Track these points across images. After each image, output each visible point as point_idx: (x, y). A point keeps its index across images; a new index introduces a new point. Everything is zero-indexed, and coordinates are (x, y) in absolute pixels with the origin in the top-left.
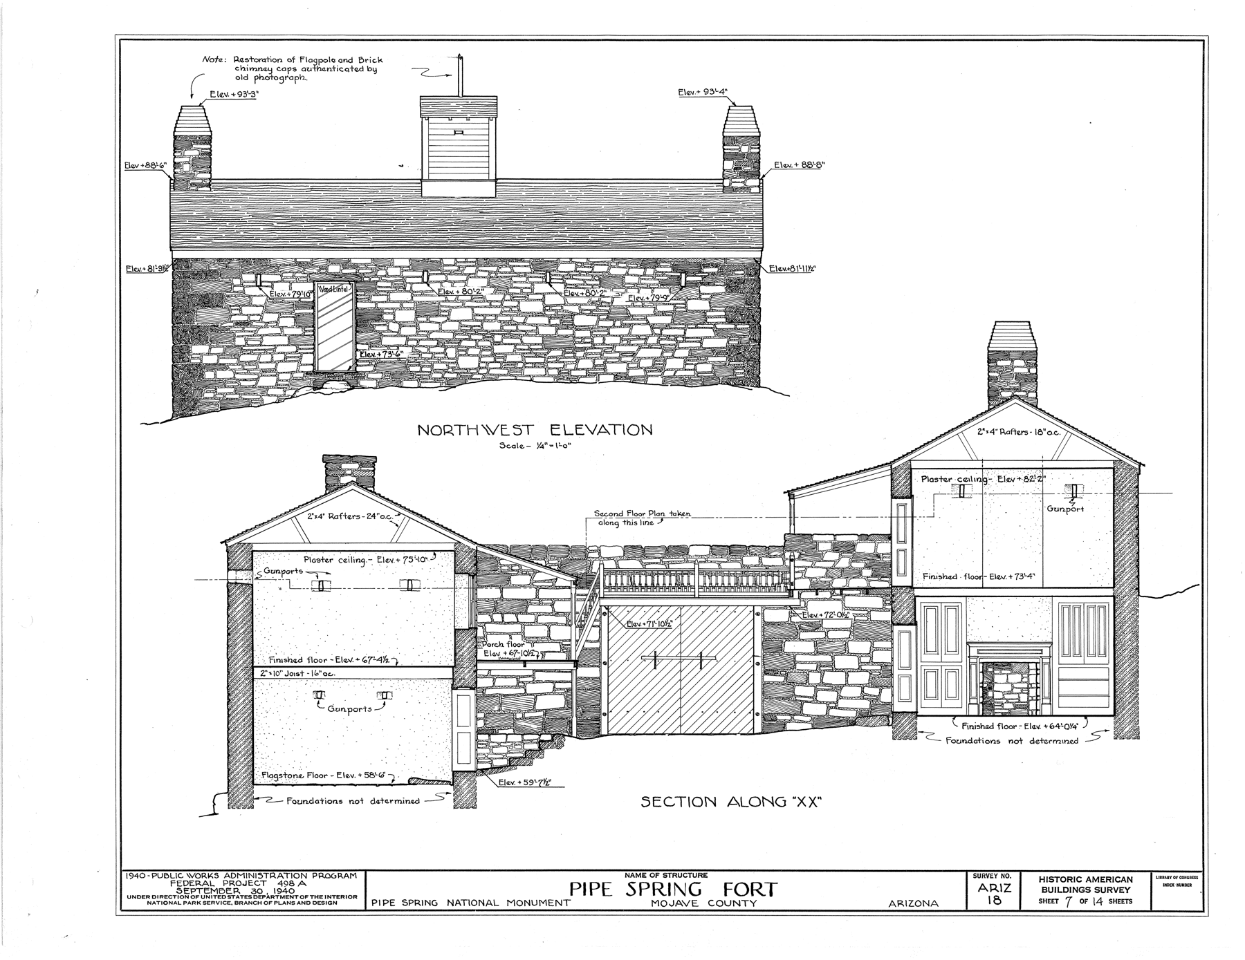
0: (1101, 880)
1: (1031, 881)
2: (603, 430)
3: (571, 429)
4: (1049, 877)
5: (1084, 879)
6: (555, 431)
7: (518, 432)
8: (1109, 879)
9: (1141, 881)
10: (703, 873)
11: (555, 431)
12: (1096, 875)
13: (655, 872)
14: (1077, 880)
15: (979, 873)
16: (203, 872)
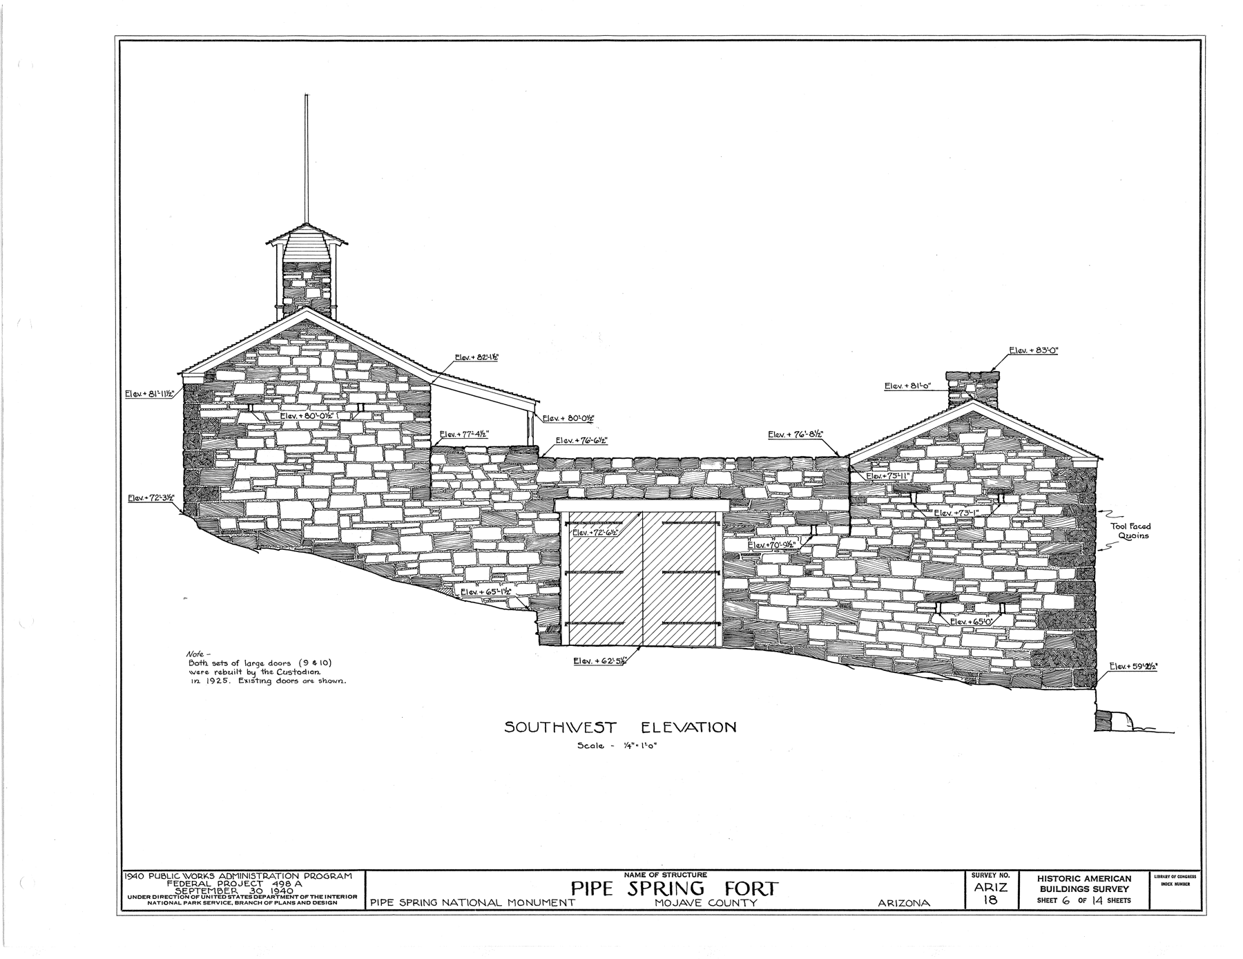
0: (1100, 879)
1: (1029, 880)
2: (689, 726)
3: (660, 727)
4: (1047, 876)
5: (1082, 878)
6: (646, 729)
7: (600, 729)
8: (1107, 878)
9: (1140, 880)
10: (702, 873)
11: (646, 729)
12: (1094, 874)
13: (655, 872)
14: (1075, 879)
15: (978, 873)
16: (200, 873)
